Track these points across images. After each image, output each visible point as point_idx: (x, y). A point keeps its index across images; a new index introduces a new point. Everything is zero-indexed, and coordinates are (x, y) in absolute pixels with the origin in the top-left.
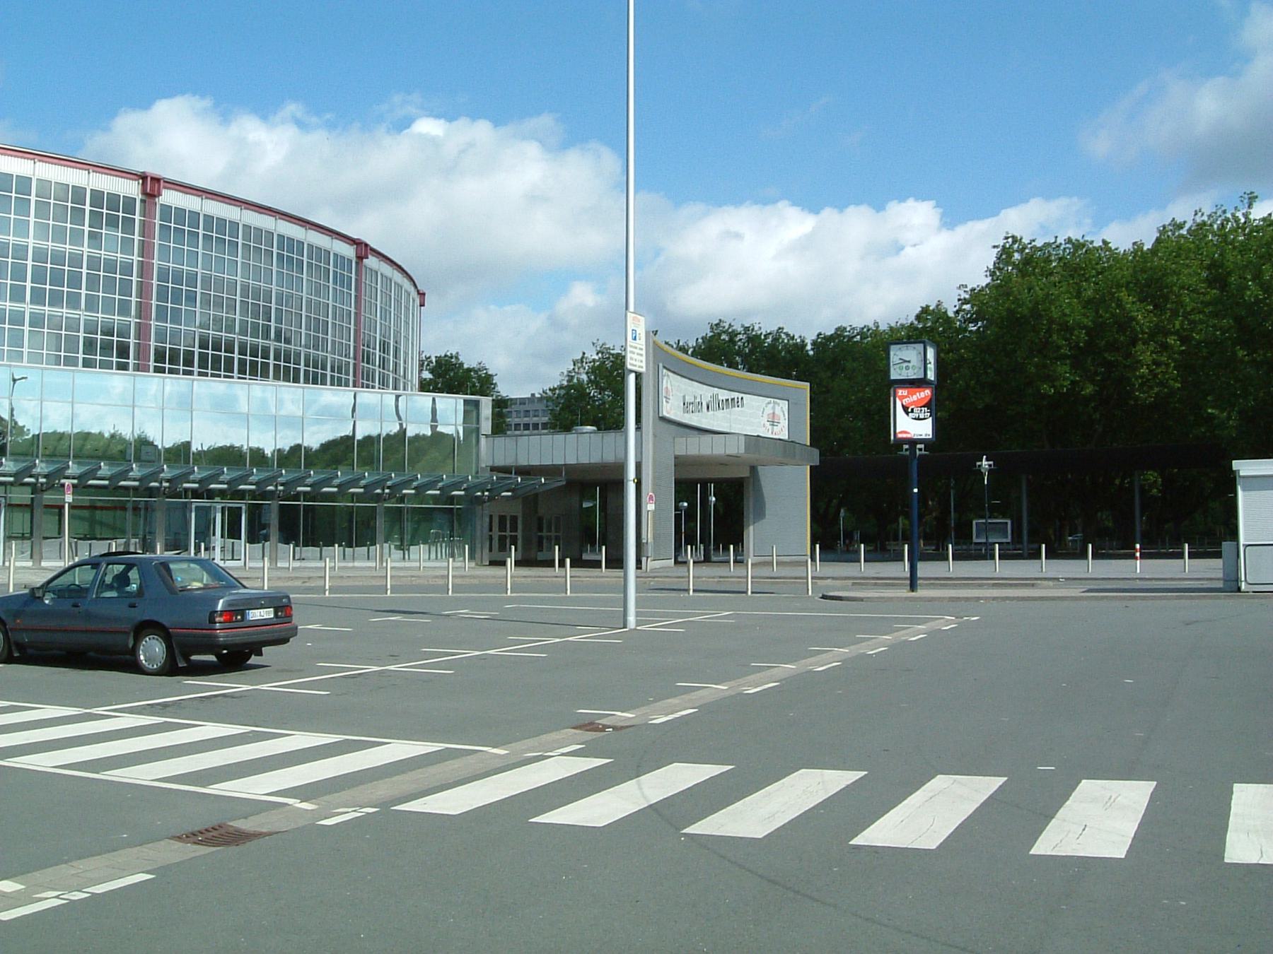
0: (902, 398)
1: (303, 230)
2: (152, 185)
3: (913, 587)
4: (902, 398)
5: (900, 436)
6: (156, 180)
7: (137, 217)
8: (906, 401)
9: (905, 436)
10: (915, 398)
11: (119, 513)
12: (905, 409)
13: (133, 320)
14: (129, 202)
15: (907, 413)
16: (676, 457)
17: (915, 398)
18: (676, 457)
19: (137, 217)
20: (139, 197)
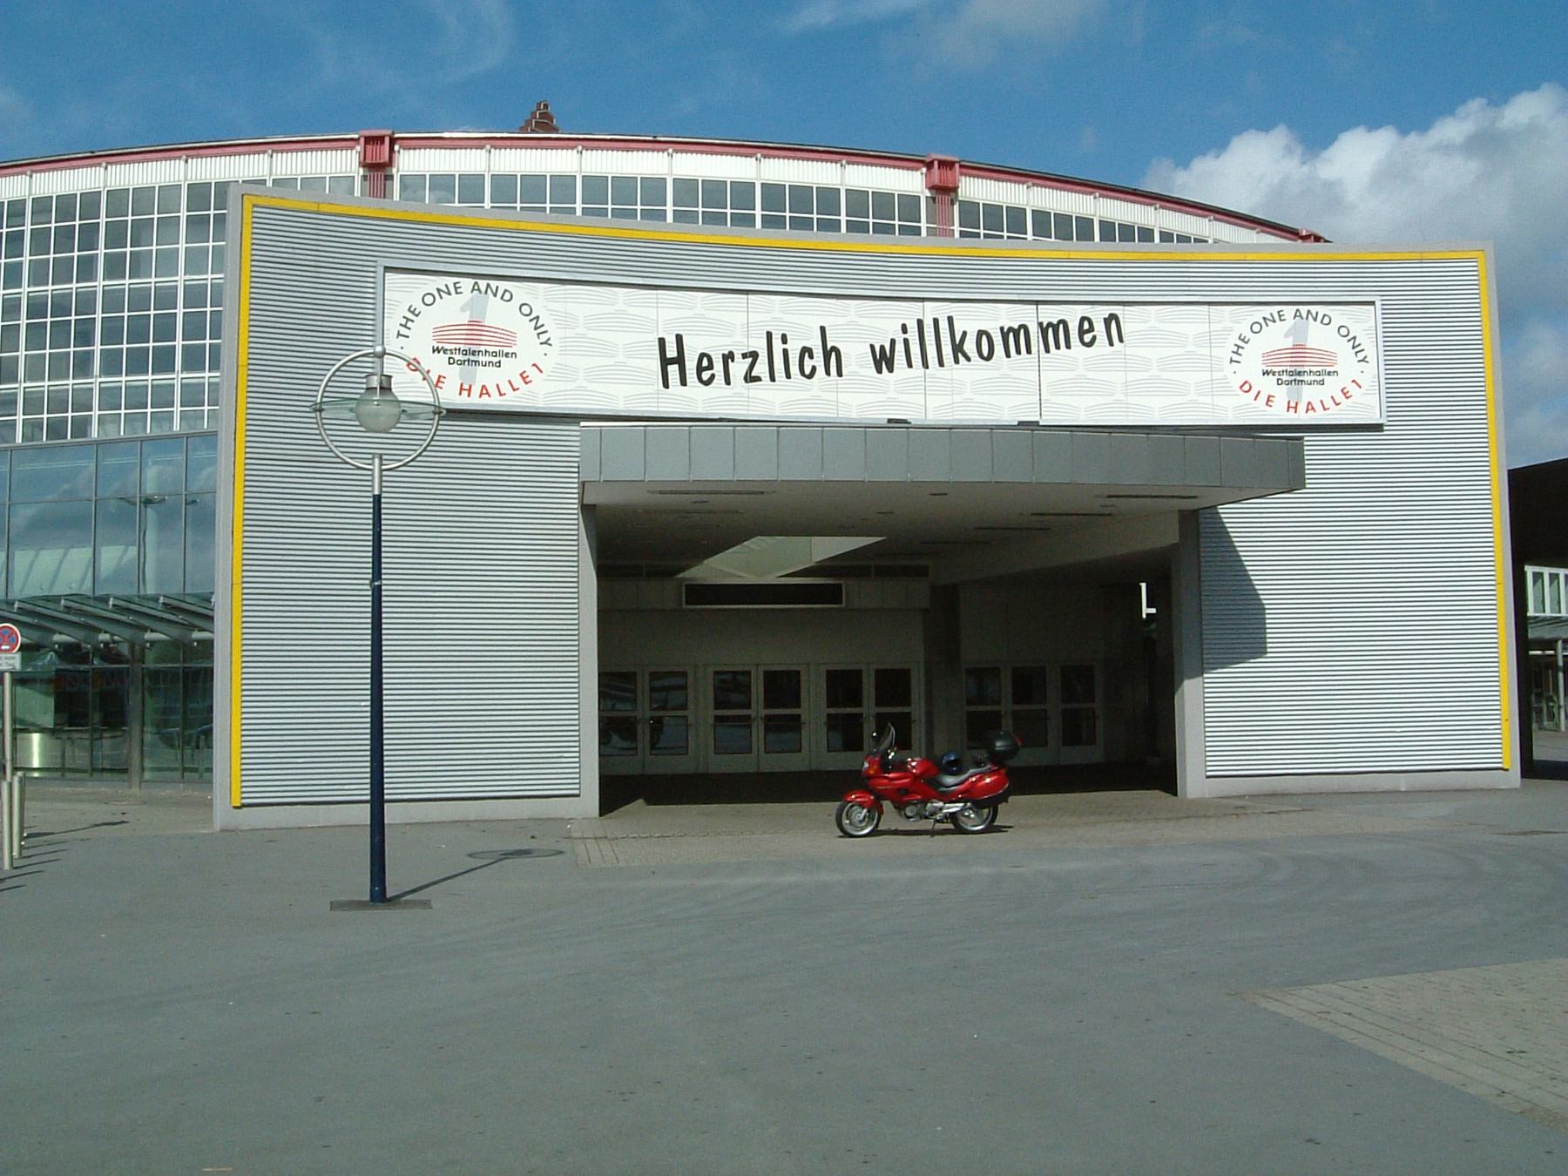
18: (587, 510)
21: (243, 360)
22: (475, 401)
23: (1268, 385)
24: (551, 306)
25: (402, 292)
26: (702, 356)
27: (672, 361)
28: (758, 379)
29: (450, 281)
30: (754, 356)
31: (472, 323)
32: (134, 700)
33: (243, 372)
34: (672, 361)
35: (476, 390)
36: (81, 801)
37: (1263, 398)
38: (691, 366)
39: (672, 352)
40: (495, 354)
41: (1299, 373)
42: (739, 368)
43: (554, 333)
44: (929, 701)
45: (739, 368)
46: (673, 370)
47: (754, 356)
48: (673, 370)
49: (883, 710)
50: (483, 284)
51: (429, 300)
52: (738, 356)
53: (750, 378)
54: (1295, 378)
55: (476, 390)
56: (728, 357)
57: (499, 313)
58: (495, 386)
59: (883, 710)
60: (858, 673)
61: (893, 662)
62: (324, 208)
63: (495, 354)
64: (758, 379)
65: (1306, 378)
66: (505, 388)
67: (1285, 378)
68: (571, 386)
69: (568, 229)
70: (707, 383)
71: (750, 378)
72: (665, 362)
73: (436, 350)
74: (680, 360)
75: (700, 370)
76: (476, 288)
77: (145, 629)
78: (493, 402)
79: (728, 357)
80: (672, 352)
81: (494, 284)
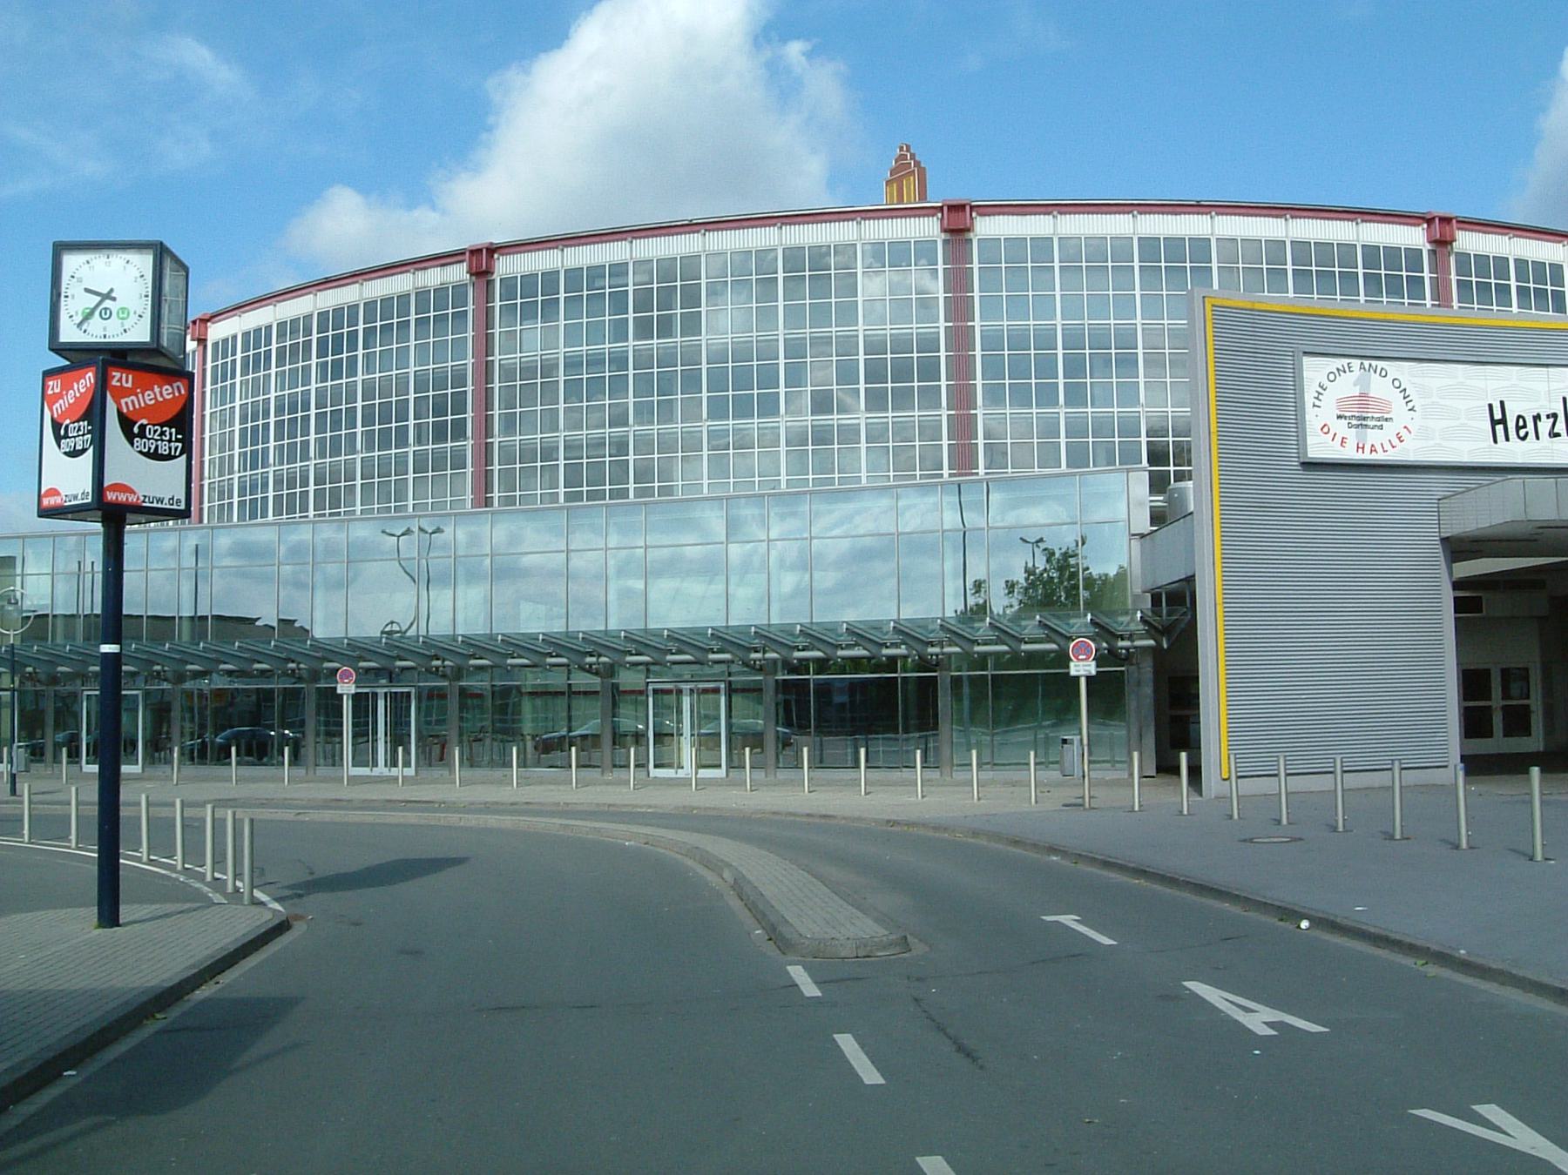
0: (121, 393)
1: (409, 276)
2: (481, 259)
3: (109, 915)
4: (121, 393)
5: (111, 496)
6: (1446, 220)
7: (1426, 274)
8: (128, 403)
9: (122, 498)
10: (148, 398)
11: (711, 696)
12: (126, 423)
13: (496, 441)
14: (1414, 255)
15: (130, 437)
16: (1444, 540)
17: (148, 398)
18: (1444, 540)
19: (1426, 274)
20: (1426, 248)
21: (1214, 428)
22: (1366, 456)
23: (1341, 427)
24: (1415, 380)
25: (1315, 370)
26: (1519, 417)
27: (1499, 422)
28: (1558, 435)
29: (1345, 361)
30: (1555, 416)
31: (1362, 395)
32: (944, 701)
33: (1214, 438)
34: (1499, 422)
35: (1368, 449)
36: (394, 810)
37: (1338, 439)
38: (1511, 425)
39: (1498, 416)
40: (1379, 419)
41: (1365, 419)
42: (1545, 426)
43: (1416, 403)
44: (1548, 692)
45: (1545, 426)
46: (1499, 428)
47: (1555, 416)
48: (1499, 428)
49: (1471, 704)
50: (1366, 363)
51: (1333, 377)
52: (1543, 418)
53: (1554, 434)
54: (1361, 423)
55: (1368, 449)
56: (1537, 418)
57: (1380, 388)
58: (1381, 445)
59: (1471, 704)
60: (1487, 672)
61: (1515, 662)
62: (1257, 306)
63: (1379, 419)
64: (1558, 435)
65: (1369, 423)
66: (1387, 446)
67: (1354, 422)
68: (1431, 443)
69: (1420, 319)
70: (1523, 439)
71: (1554, 434)
72: (1494, 423)
73: (1339, 417)
74: (1503, 421)
75: (1518, 428)
76: (1362, 367)
77: (187, 663)
78: (1380, 457)
79: (1537, 418)
80: (1498, 416)
81: (1374, 363)
